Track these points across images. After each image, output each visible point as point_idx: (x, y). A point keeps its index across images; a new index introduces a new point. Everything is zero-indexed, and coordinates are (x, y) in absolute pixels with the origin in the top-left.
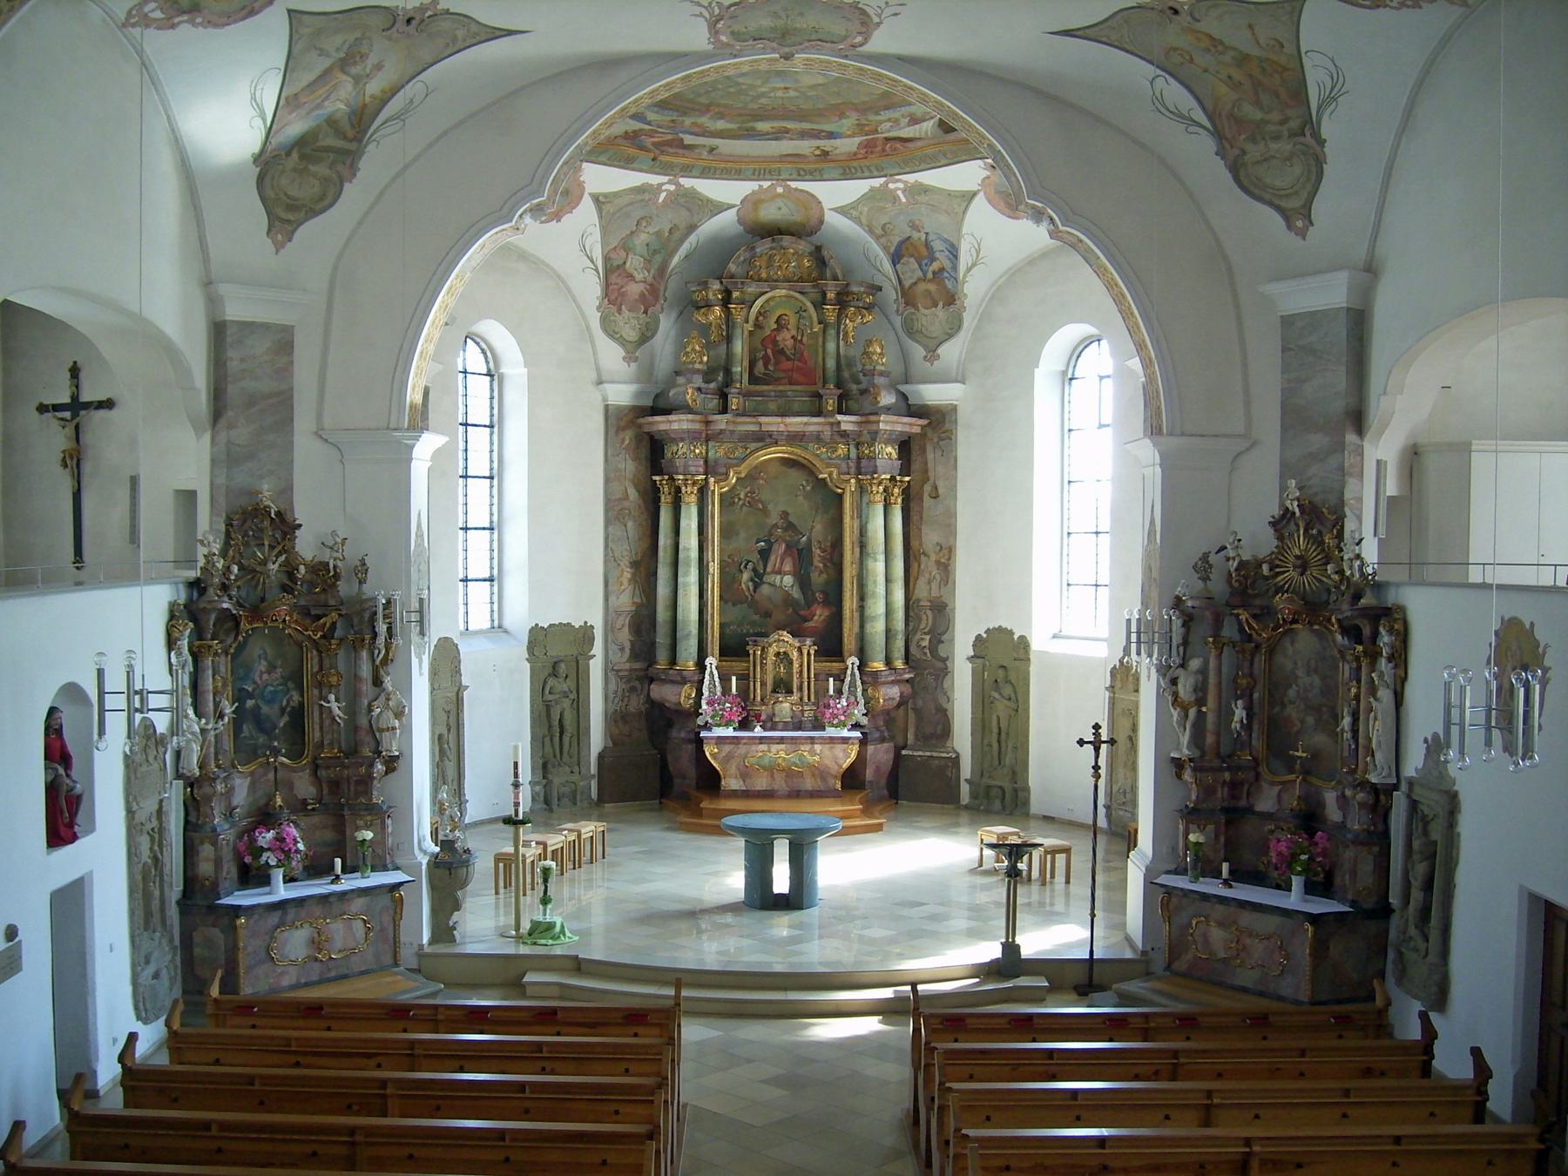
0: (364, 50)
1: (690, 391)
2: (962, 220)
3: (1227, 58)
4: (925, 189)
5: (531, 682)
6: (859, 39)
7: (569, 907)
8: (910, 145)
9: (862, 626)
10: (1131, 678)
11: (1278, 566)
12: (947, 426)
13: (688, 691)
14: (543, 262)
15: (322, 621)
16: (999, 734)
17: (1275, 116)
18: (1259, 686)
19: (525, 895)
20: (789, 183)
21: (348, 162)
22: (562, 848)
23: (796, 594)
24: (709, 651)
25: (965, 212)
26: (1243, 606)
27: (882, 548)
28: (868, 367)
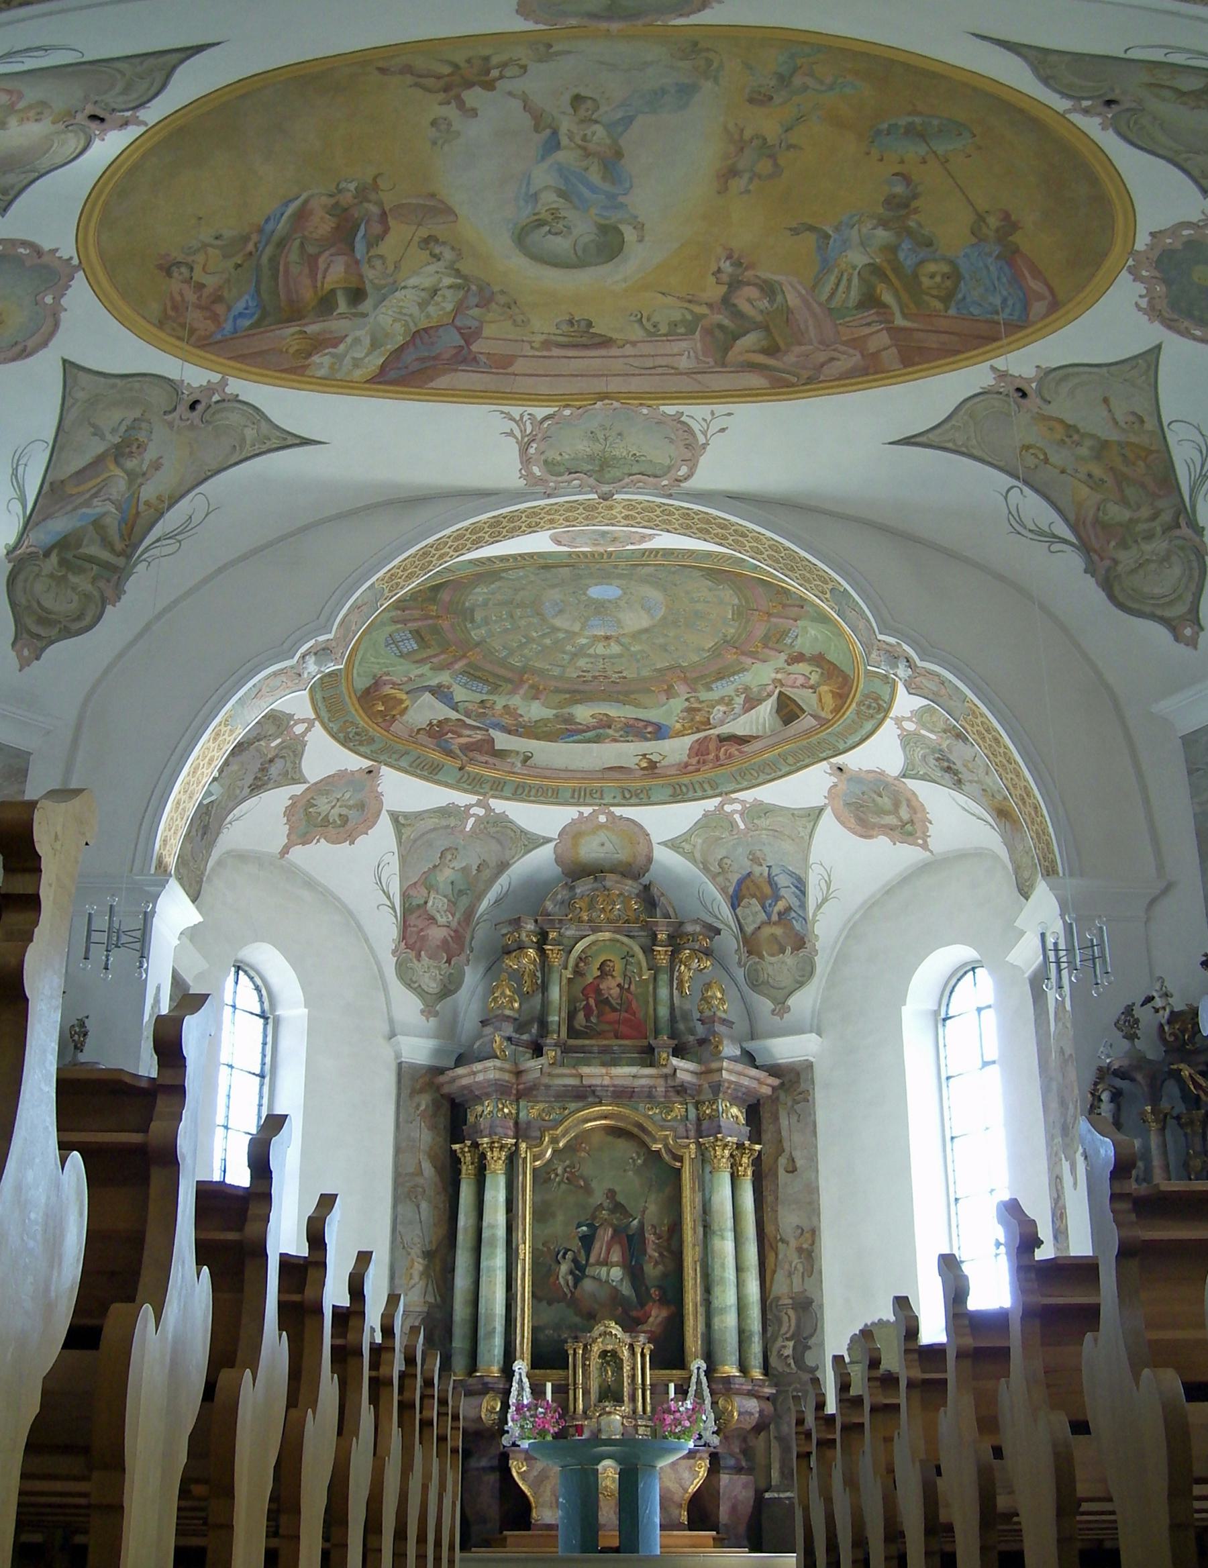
0: (142, 437)
1: (498, 1039)
2: (809, 845)
3: (1084, 451)
6: (684, 470)
8: (746, 748)
9: (708, 1325)
12: (803, 1086)
13: (489, 1406)
14: (332, 894)
17: (1145, 512)
20: (612, 809)
23: (626, 1290)
24: (518, 1354)
25: (811, 835)
27: (729, 1223)
28: (707, 1013)
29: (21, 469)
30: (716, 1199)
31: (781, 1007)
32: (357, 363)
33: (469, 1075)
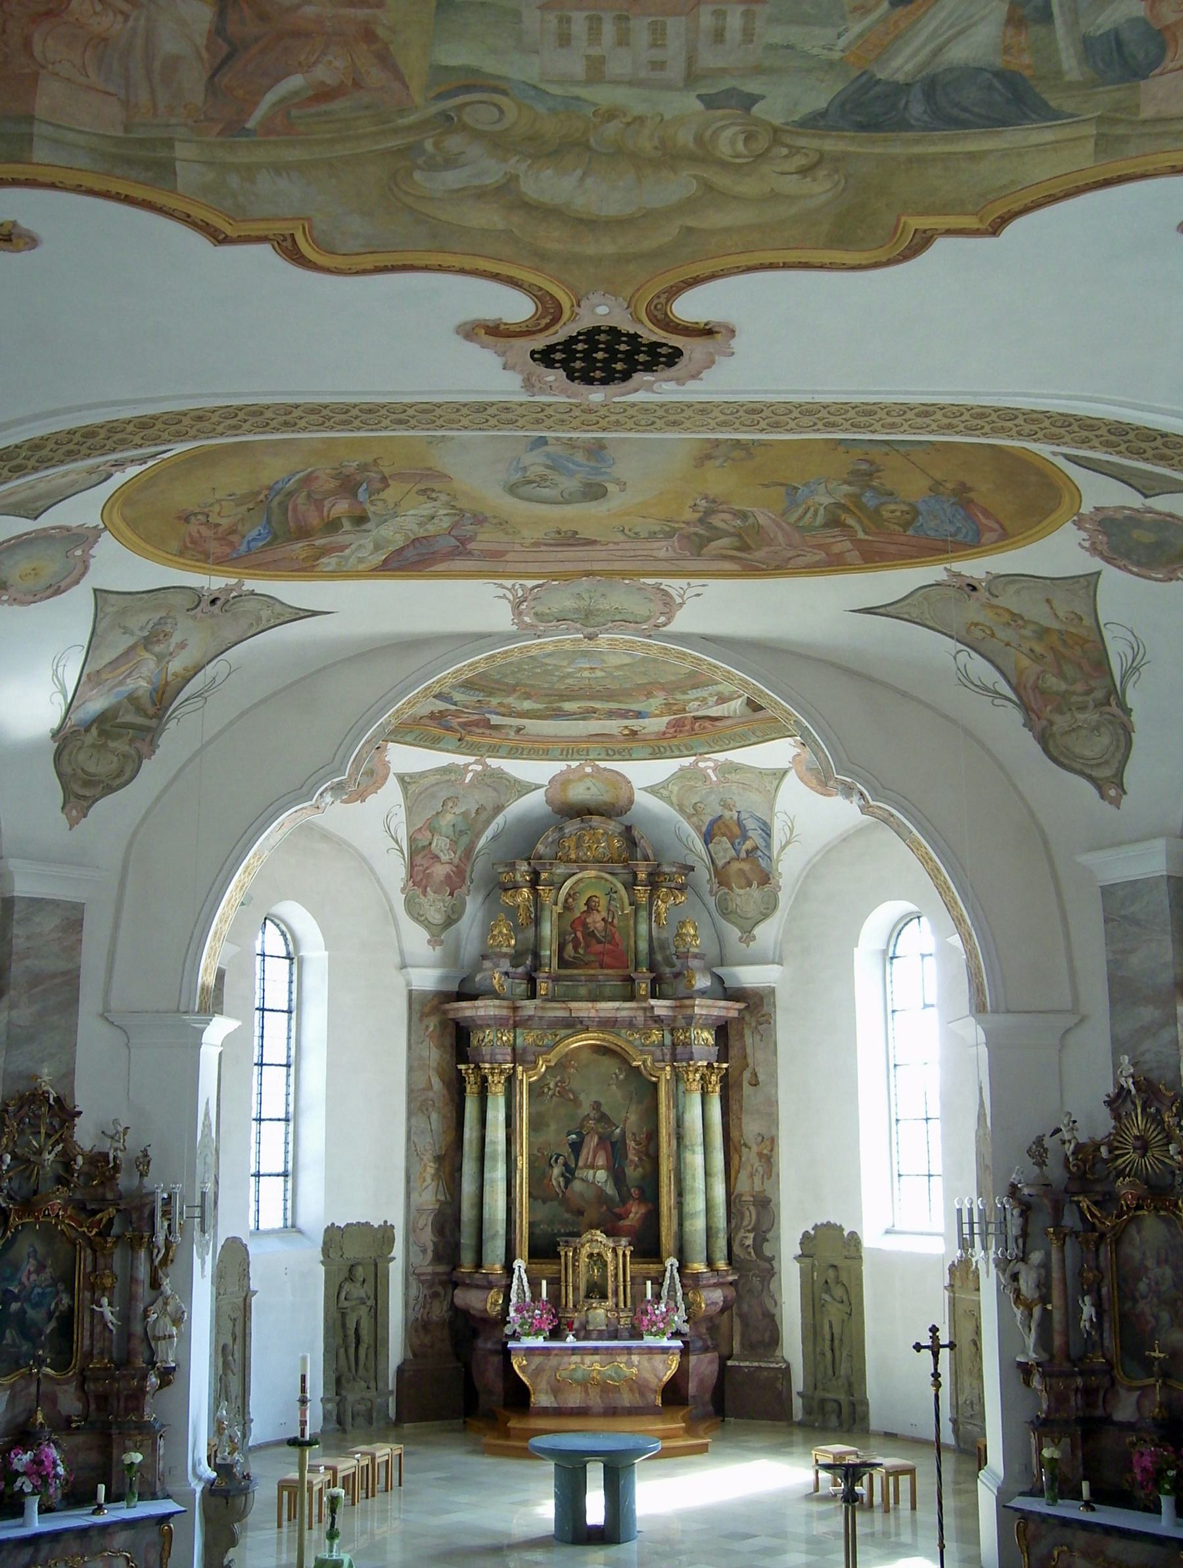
0: (168, 629)
1: (497, 976)
4: (736, 768)
5: (326, 1288)
6: (662, 619)
7: (362, 1542)
8: (717, 723)
9: (681, 1225)
10: (971, 1276)
11: (1117, 1148)
12: (765, 1009)
15: (98, 1217)
16: (832, 1340)
17: (1079, 687)
18: (1107, 1281)
19: (310, 1528)
20: (597, 763)
21: (148, 738)
22: (354, 1473)
23: (610, 1190)
24: (518, 1252)
26: (1083, 1192)
27: (700, 1139)
28: (681, 949)
29: (60, 670)
30: (687, 1117)
31: (747, 935)
32: (361, 560)
33: (471, 1008)
